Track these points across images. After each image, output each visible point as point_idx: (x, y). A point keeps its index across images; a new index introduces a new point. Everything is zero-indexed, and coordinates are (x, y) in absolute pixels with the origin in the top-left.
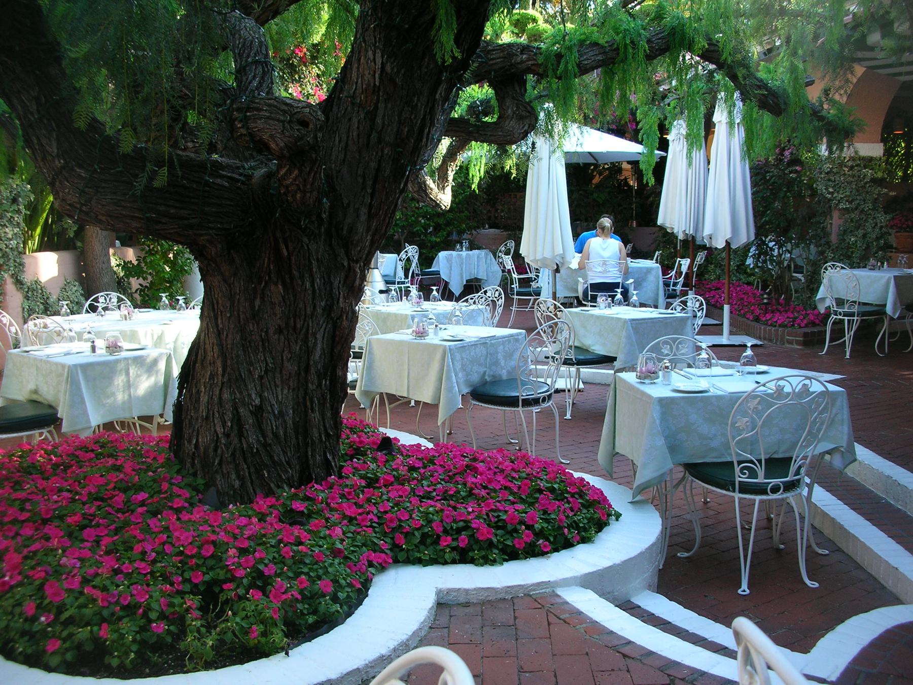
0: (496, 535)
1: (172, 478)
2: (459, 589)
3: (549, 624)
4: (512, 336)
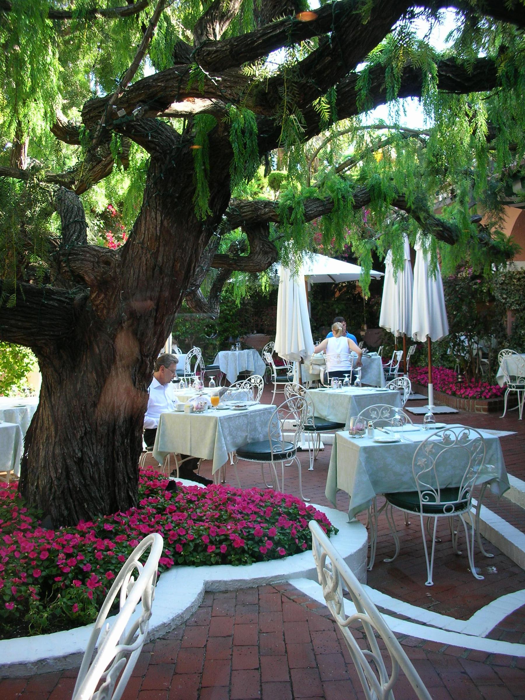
0: (247, 545)
1: (20, 510)
2: (220, 581)
3: (282, 602)
4: (266, 409)
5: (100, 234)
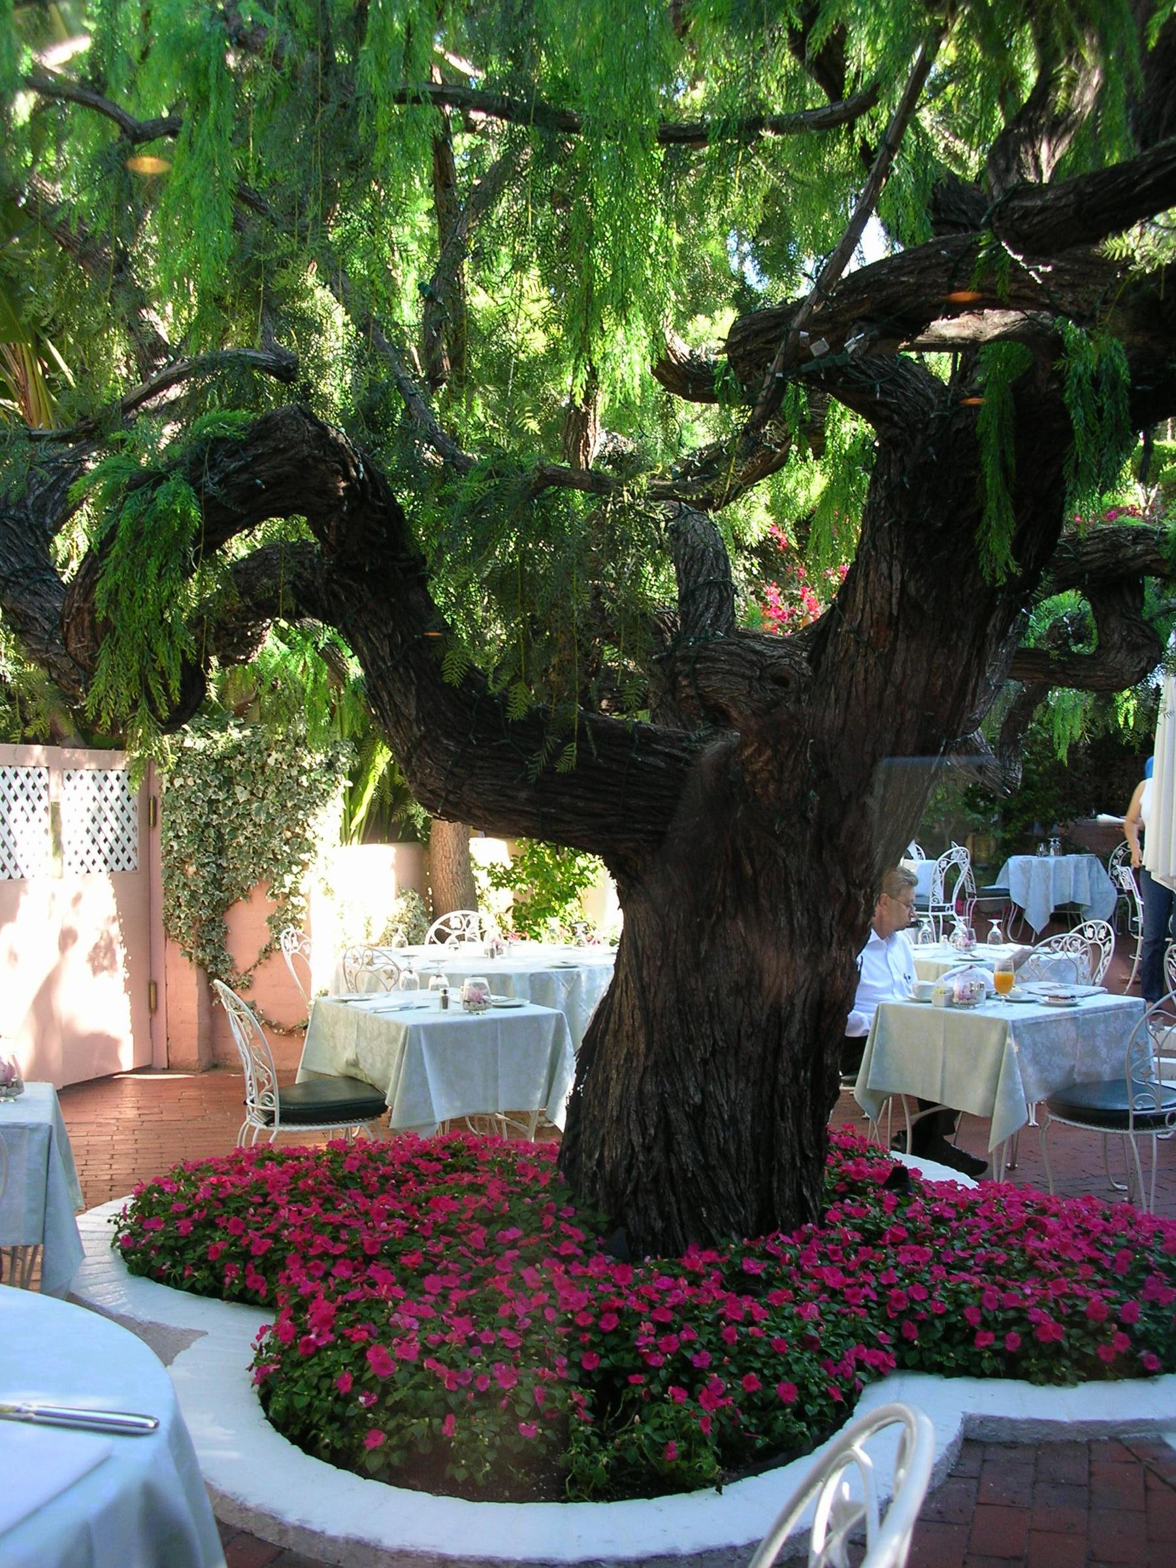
0: (1069, 1336)
2: (1001, 1418)
4: (1120, 1007)
5: (751, 589)
